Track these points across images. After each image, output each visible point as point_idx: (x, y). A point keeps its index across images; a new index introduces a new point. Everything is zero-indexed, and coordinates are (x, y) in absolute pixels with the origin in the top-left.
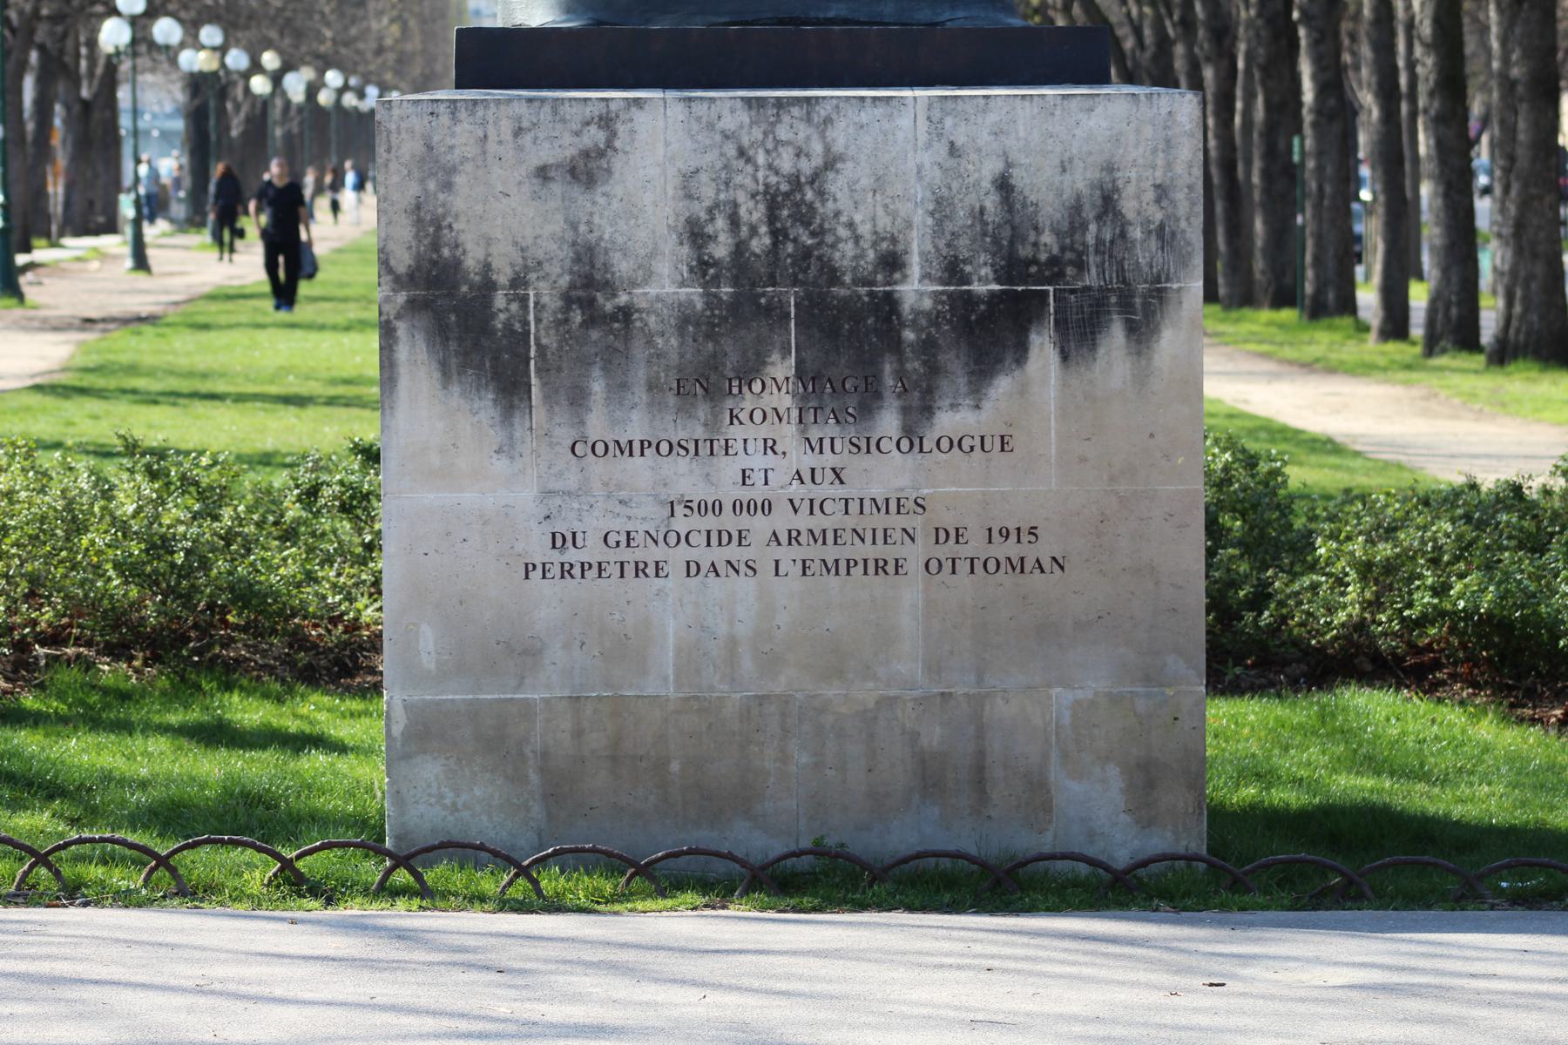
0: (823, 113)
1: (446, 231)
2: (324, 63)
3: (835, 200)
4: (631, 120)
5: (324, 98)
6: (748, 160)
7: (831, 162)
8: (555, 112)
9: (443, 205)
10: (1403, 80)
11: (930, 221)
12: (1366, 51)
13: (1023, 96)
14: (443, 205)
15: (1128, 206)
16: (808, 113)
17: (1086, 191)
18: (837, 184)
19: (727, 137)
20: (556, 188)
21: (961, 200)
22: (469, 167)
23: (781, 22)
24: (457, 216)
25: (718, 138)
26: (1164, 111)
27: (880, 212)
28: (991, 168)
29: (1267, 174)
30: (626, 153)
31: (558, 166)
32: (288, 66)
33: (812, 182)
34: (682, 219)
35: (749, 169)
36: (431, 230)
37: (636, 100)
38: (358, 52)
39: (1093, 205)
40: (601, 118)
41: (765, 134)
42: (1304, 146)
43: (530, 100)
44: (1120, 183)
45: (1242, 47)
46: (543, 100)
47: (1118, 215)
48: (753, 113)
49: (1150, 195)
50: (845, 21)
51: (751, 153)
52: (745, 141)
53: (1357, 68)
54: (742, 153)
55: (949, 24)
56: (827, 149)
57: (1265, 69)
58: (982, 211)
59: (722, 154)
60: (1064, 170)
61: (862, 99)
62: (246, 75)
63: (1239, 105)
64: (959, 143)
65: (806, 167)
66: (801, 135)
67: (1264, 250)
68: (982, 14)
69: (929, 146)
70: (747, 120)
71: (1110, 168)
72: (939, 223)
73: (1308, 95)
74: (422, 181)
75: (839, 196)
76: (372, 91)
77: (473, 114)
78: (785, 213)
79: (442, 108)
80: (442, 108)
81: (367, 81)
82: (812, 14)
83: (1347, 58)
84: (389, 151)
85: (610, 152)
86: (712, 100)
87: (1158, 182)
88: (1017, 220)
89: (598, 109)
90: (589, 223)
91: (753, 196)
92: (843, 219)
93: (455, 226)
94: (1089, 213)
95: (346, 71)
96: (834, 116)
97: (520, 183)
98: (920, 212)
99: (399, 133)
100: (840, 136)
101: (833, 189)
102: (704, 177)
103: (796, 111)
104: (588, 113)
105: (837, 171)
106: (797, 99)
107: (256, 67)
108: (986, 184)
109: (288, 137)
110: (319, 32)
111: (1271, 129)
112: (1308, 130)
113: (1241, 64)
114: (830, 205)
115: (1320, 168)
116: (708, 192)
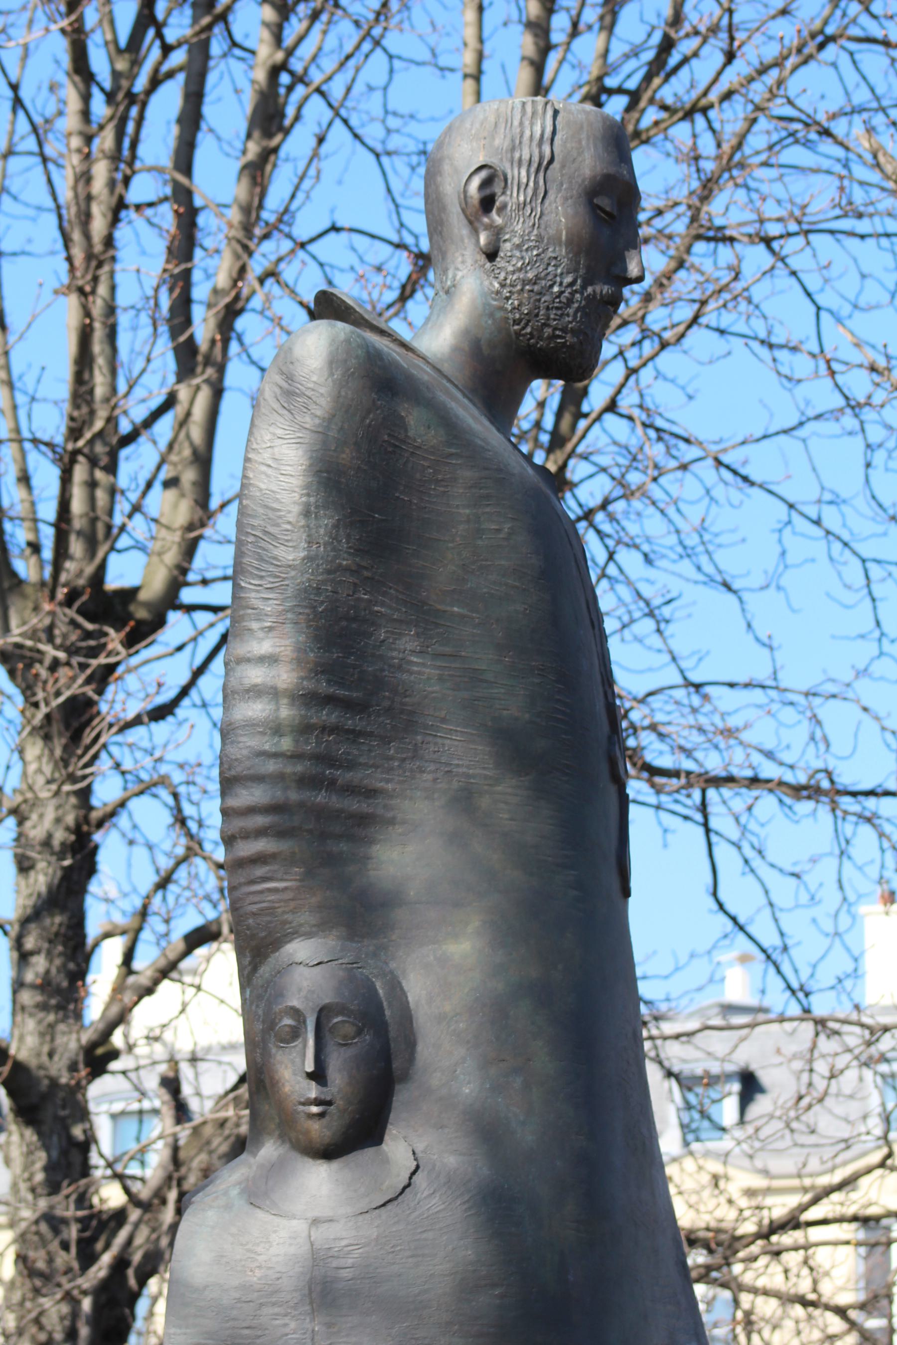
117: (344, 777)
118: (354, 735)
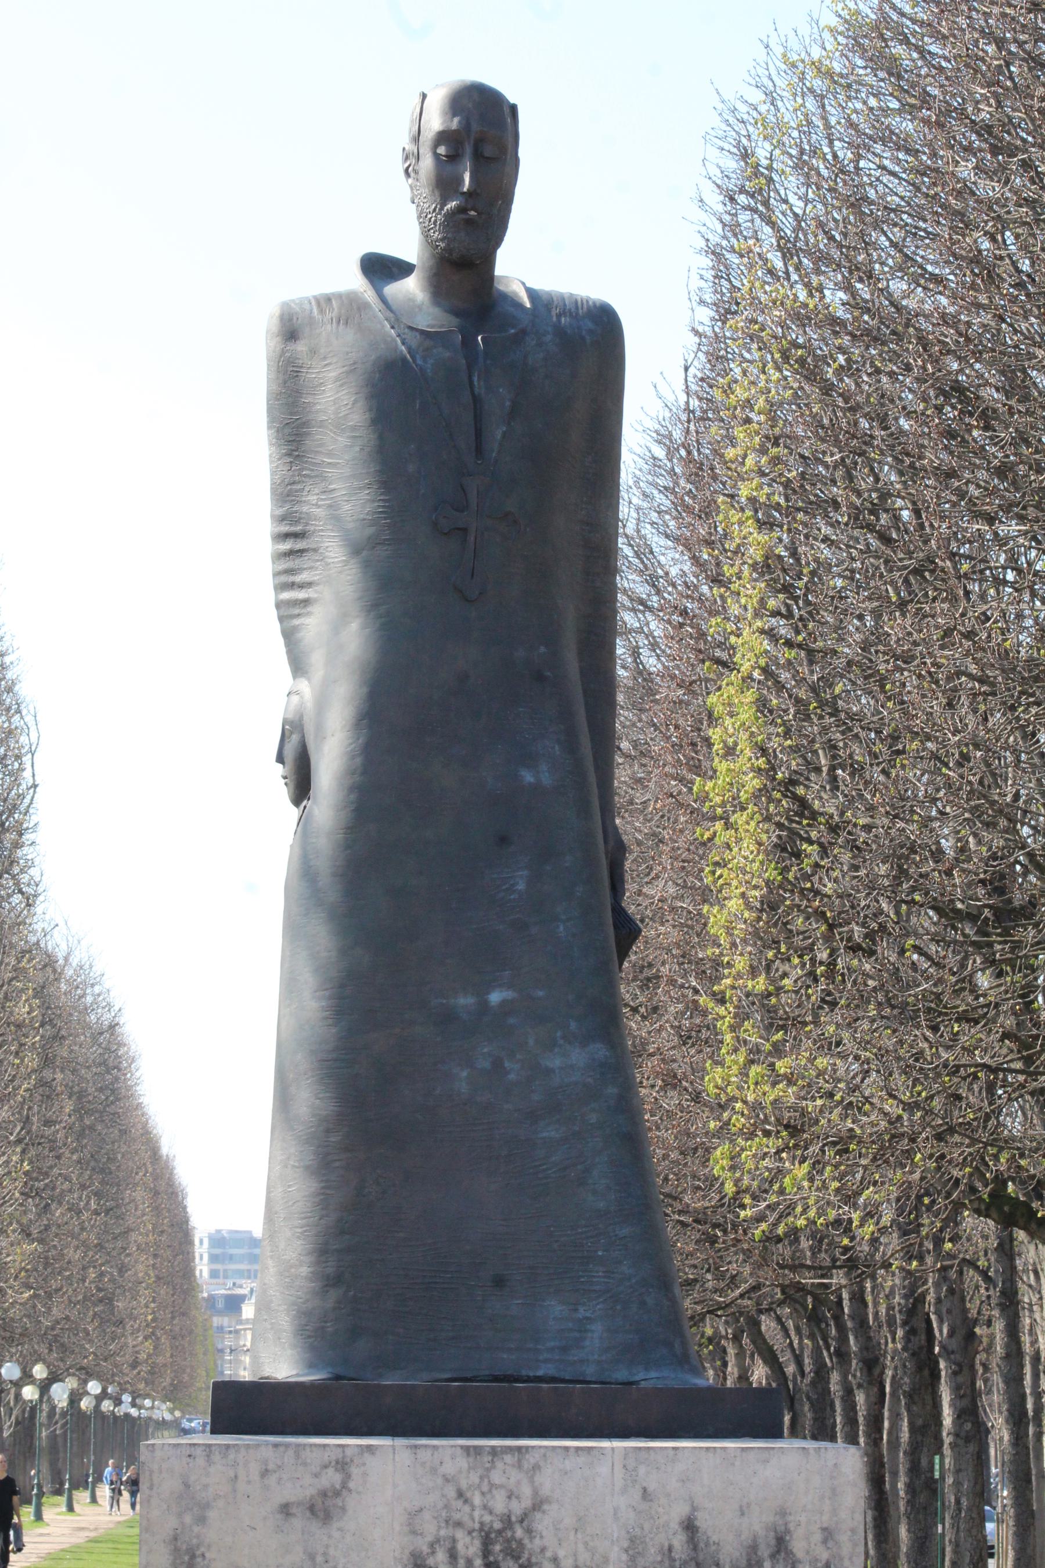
0: (532, 1461)
1: (199, 1560)
2: (87, 1374)
3: (542, 1537)
4: (364, 1464)
5: (85, 1404)
6: (466, 1501)
7: (538, 1505)
8: (297, 1456)
9: (198, 1537)
10: (1030, 1406)
11: (624, 1557)
12: (997, 1379)
13: (708, 1448)
14: (198, 1537)
15: (798, 1546)
16: (519, 1461)
17: (762, 1533)
18: (543, 1523)
19: (447, 1480)
20: (297, 1523)
21: (652, 1539)
22: (221, 1503)
23: (496, 1379)
24: (209, 1546)
25: (440, 1481)
26: (830, 1464)
27: (581, 1547)
28: (679, 1511)
29: (910, 1487)
30: (359, 1493)
31: (299, 1504)
32: (54, 1378)
33: (522, 1521)
34: (407, 1552)
35: (467, 1508)
36: (186, 1558)
37: (369, 1448)
38: (116, 1366)
39: (768, 1545)
40: (337, 1462)
41: (481, 1478)
42: (944, 1463)
43: (276, 1446)
44: (791, 1526)
45: (889, 1373)
46: (287, 1446)
47: (789, 1553)
48: (471, 1459)
49: (818, 1537)
50: (553, 1380)
51: (469, 1495)
52: (464, 1485)
53: (989, 1392)
54: (460, 1494)
55: (643, 1384)
56: (536, 1493)
57: (910, 1396)
58: (670, 1549)
59: (443, 1496)
60: (743, 1514)
61: (567, 1448)
62: (18, 1385)
63: (886, 1424)
64: (650, 1489)
65: (517, 1508)
66: (513, 1480)
67: (907, 1555)
68: (673, 1376)
69: (624, 1490)
70: (466, 1465)
71: (783, 1513)
72: (633, 1559)
73: (948, 1419)
74: (180, 1515)
75: (544, 1534)
76: (127, 1398)
77: (225, 1456)
78: (498, 1548)
79: (199, 1452)
80: (199, 1452)
81: (123, 1390)
82: (524, 1373)
83: (980, 1384)
84: (151, 1488)
85: (344, 1493)
86: (435, 1447)
87: (825, 1525)
88: (701, 1557)
89: (336, 1454)
90: (325, 1554)
91: (470, 1533)
92: (549, 1554)
93: (207, 1555)
94: (764, 1552)
95: (105, 1380)
96: (542, 1464)
97: (265, 1518)
98: (616, 1549)
99: (161, 1472)
100: (546, 1481)
101: (540, 1527)
102: (427, 1515)
103: (508, 1458)
104: (326, 1458)
105: (544, 1512)
106: (510, 1449)
107: (27, 1377)
108: (675, 1525)
109: (53, 1437)
110: (82, 1347)
111: (914, 1450)
112: (947, 1450)
113: (888, 1389)
114: (537, 1541)
115: (957, 1483)
116: (430, 1528)
117: (298, 579)
118: (301, 552)
